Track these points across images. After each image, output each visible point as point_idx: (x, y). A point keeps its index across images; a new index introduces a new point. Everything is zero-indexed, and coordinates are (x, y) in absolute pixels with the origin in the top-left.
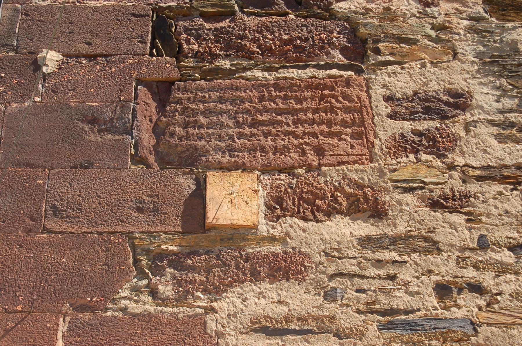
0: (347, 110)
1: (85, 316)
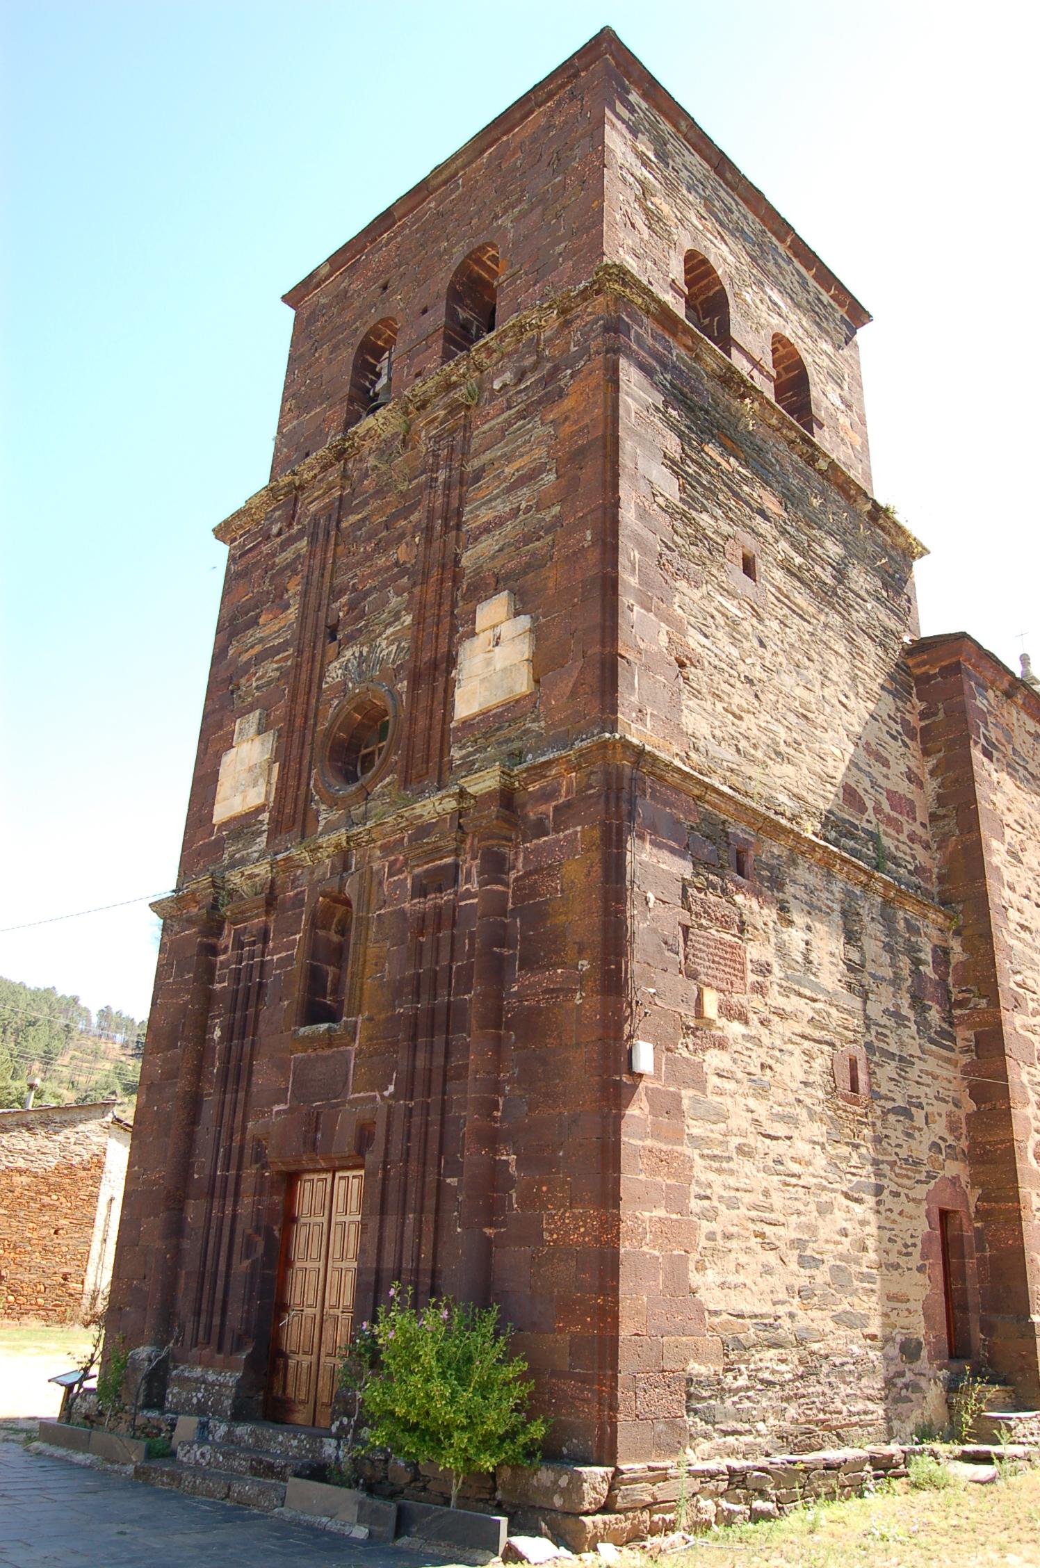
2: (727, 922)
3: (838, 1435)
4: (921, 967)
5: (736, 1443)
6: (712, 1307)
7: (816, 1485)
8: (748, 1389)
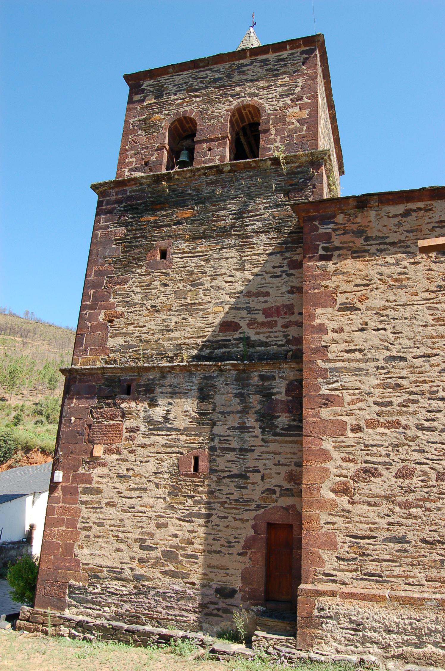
0: (119, 431)
1: (75, 473)
2: (113, 417)
3: (158, 622)
4: (273, 397)
5: (92, 612)
6: (84, 562)
7: (119, 636)
8: (100, 594)
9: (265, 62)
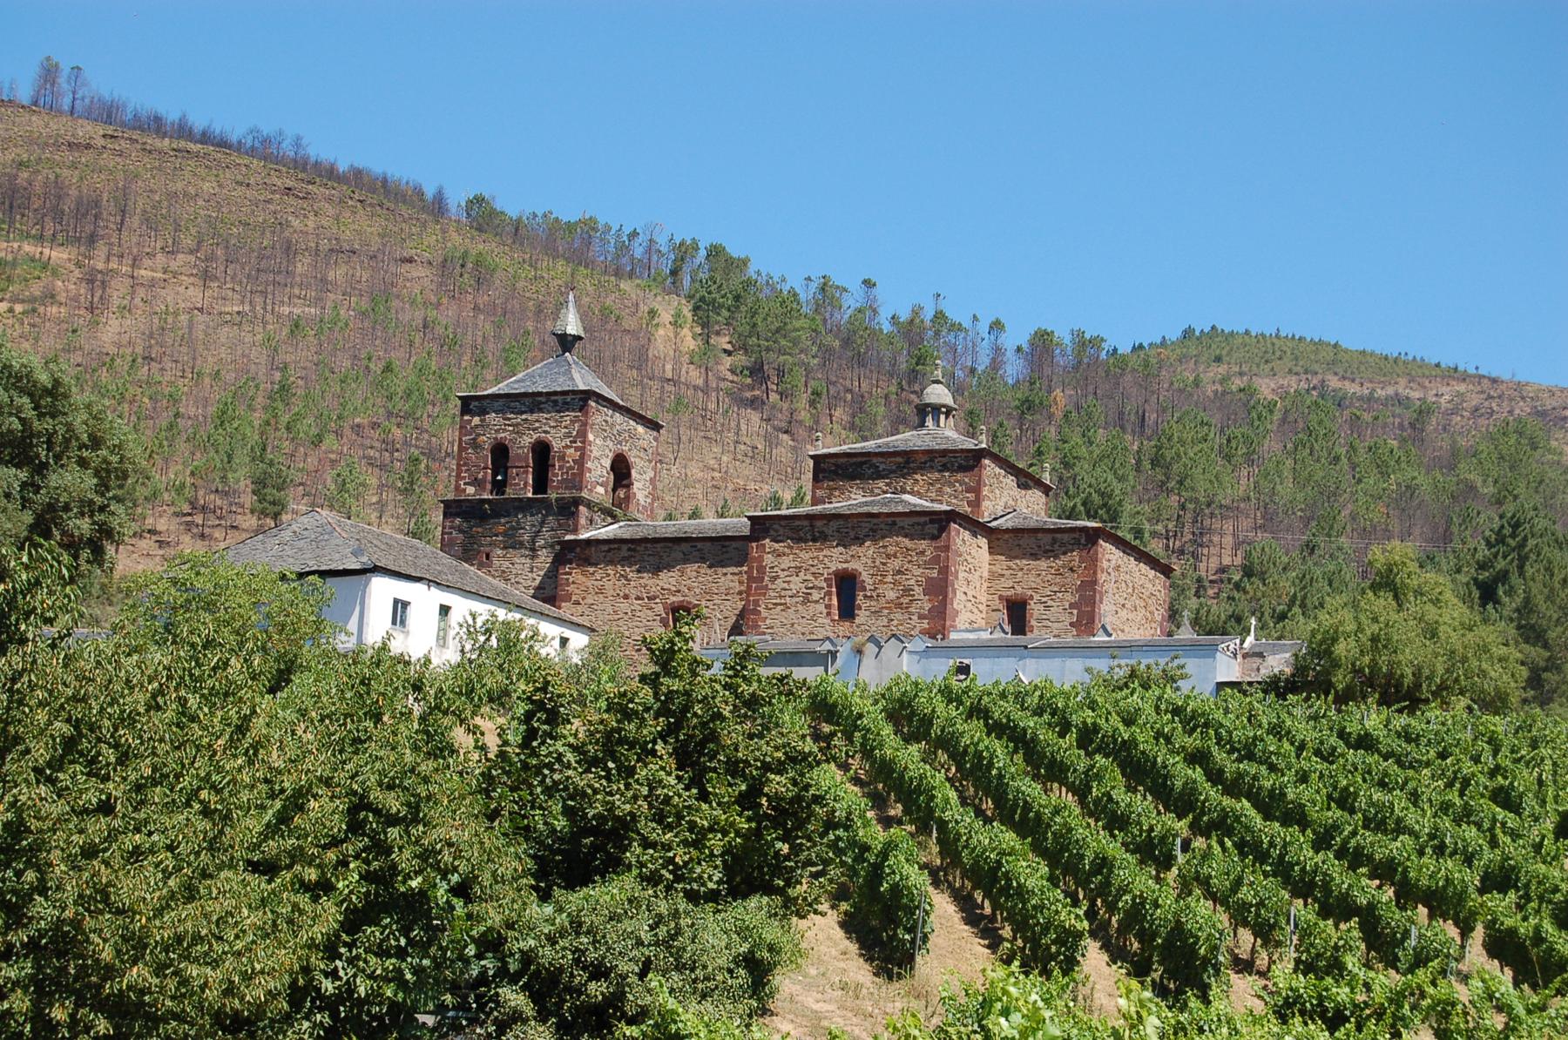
9: (555, 402)
